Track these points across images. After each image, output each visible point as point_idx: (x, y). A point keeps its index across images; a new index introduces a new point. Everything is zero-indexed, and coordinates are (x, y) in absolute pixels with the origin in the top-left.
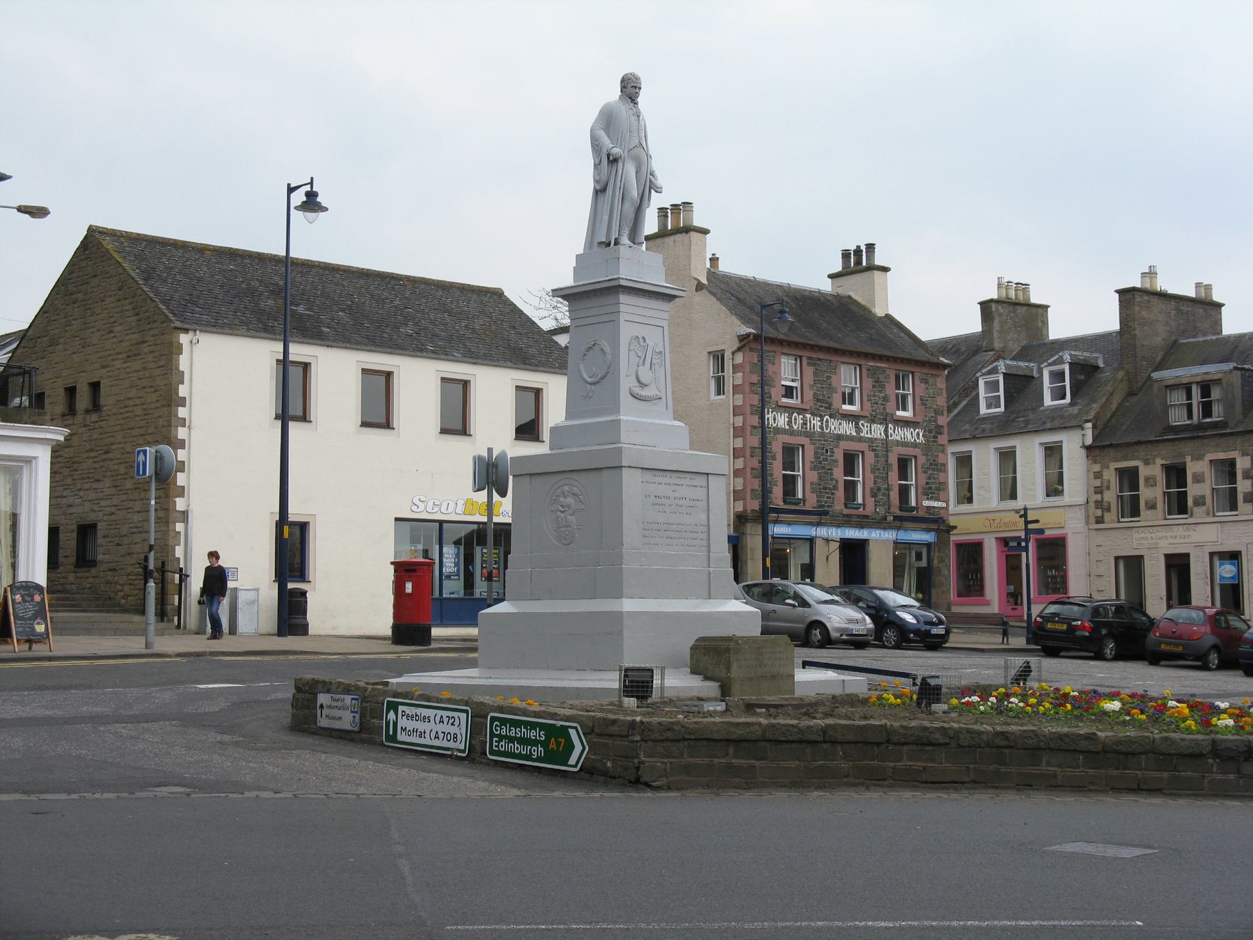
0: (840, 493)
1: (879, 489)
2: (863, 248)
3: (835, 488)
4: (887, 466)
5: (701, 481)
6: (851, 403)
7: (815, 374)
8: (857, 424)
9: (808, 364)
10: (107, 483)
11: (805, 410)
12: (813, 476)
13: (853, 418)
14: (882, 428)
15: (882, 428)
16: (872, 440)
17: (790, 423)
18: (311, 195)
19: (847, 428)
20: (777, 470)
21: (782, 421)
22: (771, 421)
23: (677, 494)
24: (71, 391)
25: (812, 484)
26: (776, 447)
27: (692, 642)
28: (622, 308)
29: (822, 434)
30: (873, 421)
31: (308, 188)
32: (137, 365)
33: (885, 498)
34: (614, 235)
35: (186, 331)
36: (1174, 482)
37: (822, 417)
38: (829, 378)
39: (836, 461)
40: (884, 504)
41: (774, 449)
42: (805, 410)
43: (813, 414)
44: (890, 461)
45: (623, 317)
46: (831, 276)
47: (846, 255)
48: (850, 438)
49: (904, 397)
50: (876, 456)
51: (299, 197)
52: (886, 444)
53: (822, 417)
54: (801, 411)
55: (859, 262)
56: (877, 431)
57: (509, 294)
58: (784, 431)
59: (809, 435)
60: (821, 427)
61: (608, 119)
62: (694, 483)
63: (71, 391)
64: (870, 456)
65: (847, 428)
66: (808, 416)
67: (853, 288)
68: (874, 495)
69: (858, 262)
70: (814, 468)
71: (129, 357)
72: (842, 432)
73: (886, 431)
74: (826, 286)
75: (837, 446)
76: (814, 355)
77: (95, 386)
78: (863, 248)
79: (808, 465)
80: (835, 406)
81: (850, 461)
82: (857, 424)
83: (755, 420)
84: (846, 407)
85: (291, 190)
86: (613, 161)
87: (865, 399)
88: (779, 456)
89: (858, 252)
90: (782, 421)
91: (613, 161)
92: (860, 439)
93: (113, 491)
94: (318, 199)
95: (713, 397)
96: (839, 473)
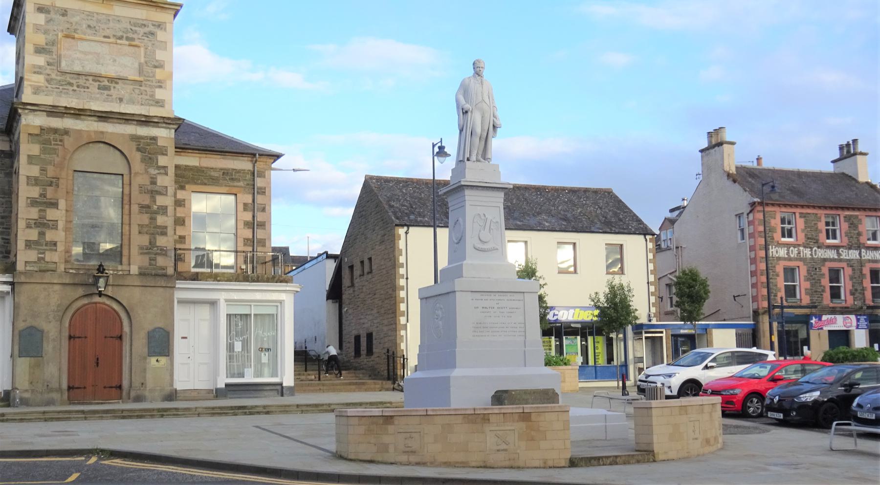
0: (827, 294)
1: (856, 290)
2: (851, 142)
3: (823, 291)
4: (862, 276)
5: (520, 296)
6: (835, 238)
7: (806, 223)
8: (838, 251)
9: (800, 217)
10: (375, 311)
11: (799, 245)
12: (807, 285)
13: (836, 247)
14: (857, 252)
15: (857, 252)
16: (849, 260)
17: (788, 253)
18: (441, 148)
19: (831, 254)
20: (781, 283)
21: (782, 252)
22: (775, 253)
23: (499, 306)
24: (362, 262)
25: (806, 289)
26: (780, 269)
27: (493, 393)
28: (467, 198)
29: (812, 259)
30: (850, 249)
31: (439, 144)
32: (383, 247)
33: (861, 296)
34: (467, 155)
35: (402, 226)
36: (789, 277)
37: (811, 248)
38: (815, 224)
39: (824, 275)
40: (860, 299)
41: (777, 270)
42: (799, 245)
43: (805, 247)
44: (864, 272)
45: (467, 203)
46: (834, 162)
47: (841, 148)
48: (833, 260)
49: (834, 231)
50: (853, 270)
51: (436, 150)
52: (861, 262)
53: (811, 248)
54: (795, 246)
55: (848, 151)
56: (854, 254)
57: (616, 192)
58: (785, 259)
59: (804, 260)
60: (811, 255)
61: (464, 90)
62: (513, 298)
63: (362, 262)
64: (849, 271)
65: (831, 254)
66: (801, 248)
67: (845, 167)
68: (852, 294)
69: (848, 152)
70: (807, 279)
71: (382, 242)
72: (826, 256)
73: (860, 254)
74: (830, 168)
75: (824, 265)
76: (805, 211)
77: (370, 259)
78: (851, 142)
79: (802, 278)
80: (821, 241)
81: (835, 275)
82: (838, 251)
83: (762, 253)
84: (831, 241)
85: (434, 146)
86: (466, 112)
87: (843, 235)
88: (782, 274)
89: (848, 145)
90: (782, 252)
91: (466, 112)
92: (840, 260)
93: (377, 315)
94: (445, 150)
95: (740, 241)
96: (826, 282)
